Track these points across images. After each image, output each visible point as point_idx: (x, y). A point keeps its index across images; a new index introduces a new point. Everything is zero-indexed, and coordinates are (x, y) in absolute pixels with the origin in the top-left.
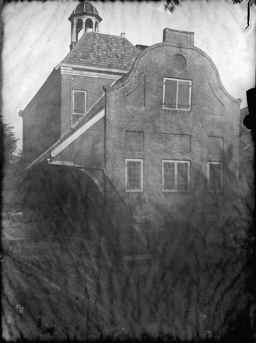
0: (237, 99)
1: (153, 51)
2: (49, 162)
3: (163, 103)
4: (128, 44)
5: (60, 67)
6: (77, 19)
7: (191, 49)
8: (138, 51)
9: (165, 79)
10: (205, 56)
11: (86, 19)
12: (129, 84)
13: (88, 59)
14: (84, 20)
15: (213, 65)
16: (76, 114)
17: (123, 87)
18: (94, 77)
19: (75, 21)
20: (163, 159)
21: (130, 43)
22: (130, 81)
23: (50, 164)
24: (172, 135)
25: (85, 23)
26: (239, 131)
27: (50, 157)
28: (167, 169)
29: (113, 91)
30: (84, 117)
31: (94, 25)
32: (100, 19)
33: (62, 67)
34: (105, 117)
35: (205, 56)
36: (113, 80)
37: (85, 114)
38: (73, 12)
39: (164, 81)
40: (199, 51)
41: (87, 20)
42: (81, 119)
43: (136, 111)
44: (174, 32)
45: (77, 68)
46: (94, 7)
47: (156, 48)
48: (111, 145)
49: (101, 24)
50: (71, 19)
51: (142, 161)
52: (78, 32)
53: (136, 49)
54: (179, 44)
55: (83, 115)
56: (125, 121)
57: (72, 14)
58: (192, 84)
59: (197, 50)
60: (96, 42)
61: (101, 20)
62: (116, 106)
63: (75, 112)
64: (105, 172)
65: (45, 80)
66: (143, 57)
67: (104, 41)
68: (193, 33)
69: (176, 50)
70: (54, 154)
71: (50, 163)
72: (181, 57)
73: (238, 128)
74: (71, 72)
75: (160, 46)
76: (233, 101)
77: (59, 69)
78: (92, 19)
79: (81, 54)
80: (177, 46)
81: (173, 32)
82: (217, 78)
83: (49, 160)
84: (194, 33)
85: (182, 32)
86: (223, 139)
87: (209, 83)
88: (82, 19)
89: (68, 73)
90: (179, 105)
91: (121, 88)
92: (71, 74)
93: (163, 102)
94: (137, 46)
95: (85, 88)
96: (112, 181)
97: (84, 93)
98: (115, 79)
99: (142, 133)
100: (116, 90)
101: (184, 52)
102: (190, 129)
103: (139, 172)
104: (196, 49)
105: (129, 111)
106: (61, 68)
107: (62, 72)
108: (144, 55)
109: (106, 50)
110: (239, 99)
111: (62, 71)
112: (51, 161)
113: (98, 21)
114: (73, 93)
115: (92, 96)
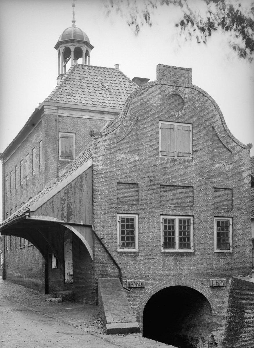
0: (247, 145)
1: (145, 91)
2: (27, 217)
5: (43, 107)
6: (64, 47)
7: (189, 88)
8: (135, 85)
9: (161, 122)
10: (205, 96)
12: (120, 130)
14: (72, 49)
15: (216, 107)
16: (62, 160)
17: (112, 133)
18: (84, 117)
19: (62, 50)
22: (120, 126)
23: (28, 219)
24: (172, 187)
26: (250, 181)
28: (167, 225)
29: (101, 137)
31: (84, 54)
32: (92, 47)
33: (46, 106)
35: (205, 96)
36: (107, 121)
39: (160, 125)
40: (199, 90)
43: (129, 160)
44: (169, 68)
45: (63, 107)
47: (149, 87)
49: (92, 53)
50: (57, 47)
51: (137, 216)
52: (66, 62)
54: (175, 83)
55: (72, 162)
59: (197, 89)
61: (93, 48)
62: (104, 154)
63: (62, 158)
66: (135, 98)
68: (191, 69)
69: (171, 90)
71: (29, 218)
73: (250, 178)
74: (56, 111)
75: (153, 84)
76: (241, 147)
77: (42, 109)
78: (81, 48)
80: (173, 85)
82: (222, 122)
83: (27, 214)
84: (191, 69)
85: (178, 68)
87: (213, 127)
88: (70, 47)
89: (52, 113)
90: (178, 153)
91: (110, 133)
93: (160, 150)
94: (135, 79)
95: (73, 130)
96: (102, 239)
97: (73, 135)
98: (108, 119)
100: (105, 136)
101: (182, 91)
102: (192, 180)
103: (228, 229)
104: (195, 88)
105: (120, 159)
106: (45, 107)
107: (46, 112)
108: (135, 96)
111: (45, 110)
112: (29, 216)
113: (89, 49)
115: (81, 139)
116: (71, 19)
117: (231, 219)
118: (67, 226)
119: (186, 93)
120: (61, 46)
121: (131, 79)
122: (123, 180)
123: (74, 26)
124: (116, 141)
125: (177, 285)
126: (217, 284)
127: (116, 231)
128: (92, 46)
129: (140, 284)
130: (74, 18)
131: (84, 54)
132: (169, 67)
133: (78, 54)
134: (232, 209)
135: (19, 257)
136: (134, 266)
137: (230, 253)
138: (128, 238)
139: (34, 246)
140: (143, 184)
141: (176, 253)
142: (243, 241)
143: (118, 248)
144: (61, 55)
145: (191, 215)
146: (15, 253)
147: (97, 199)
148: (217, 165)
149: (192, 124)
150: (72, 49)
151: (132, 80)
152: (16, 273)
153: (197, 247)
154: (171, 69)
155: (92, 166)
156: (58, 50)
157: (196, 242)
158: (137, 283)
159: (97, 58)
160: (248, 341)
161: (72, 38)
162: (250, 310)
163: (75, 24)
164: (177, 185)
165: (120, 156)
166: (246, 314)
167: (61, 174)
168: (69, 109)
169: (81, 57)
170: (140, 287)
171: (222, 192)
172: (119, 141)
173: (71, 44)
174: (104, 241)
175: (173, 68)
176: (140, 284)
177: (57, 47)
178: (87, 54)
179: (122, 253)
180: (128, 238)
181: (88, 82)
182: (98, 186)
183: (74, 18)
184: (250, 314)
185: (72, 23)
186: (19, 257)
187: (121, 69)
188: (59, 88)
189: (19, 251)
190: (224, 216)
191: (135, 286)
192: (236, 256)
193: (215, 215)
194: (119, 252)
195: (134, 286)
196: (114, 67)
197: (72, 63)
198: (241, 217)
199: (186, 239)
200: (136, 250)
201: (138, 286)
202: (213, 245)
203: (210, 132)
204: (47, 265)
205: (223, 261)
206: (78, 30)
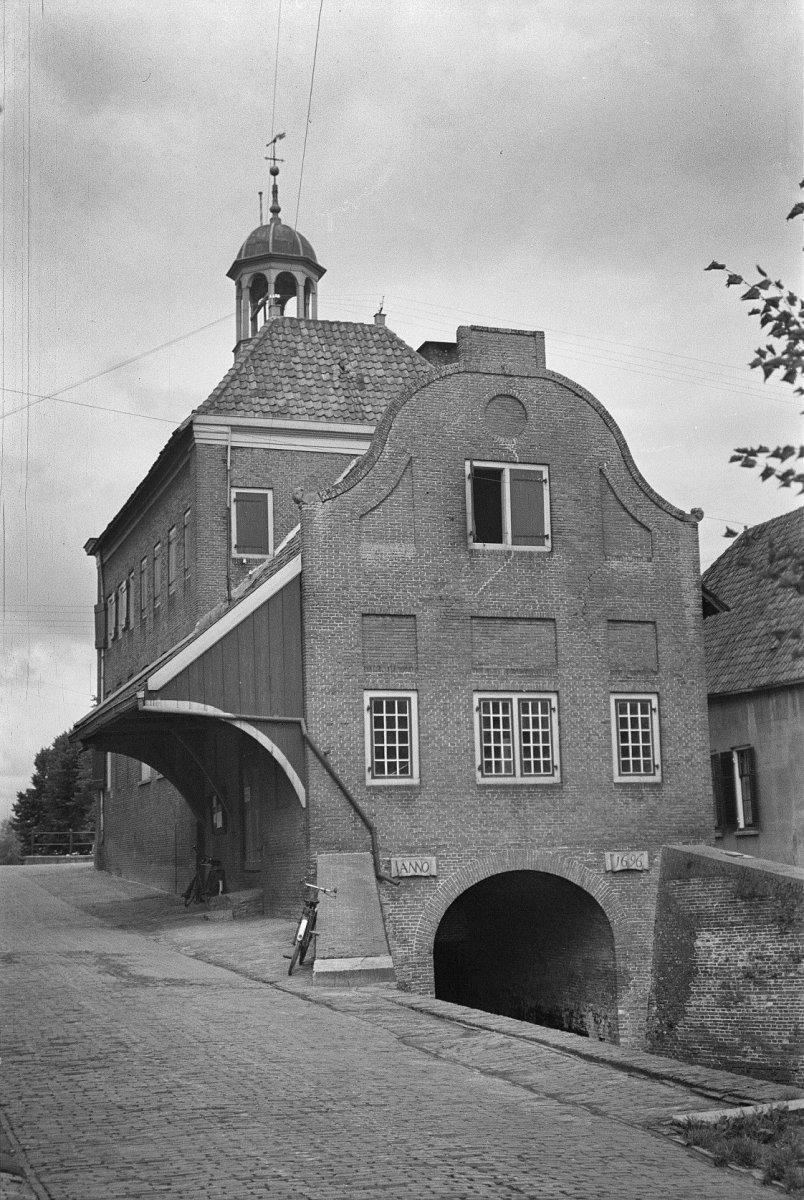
3: (469, 532)
4: (395, 344)
11: (278, 272)
13: (274, 399)
14: (272, 275)
19: (246, 280)
20: (478, 691)
21: (401, 343)
25: (276, 285)
27: (146, 690)
30: (265, 565)
31: (301, 290)
32: (321, 272)
34: (299, 580)
37: (269, 558)
38: (240, 255)
41: (279, 277)
42: (255, 571)
46: (300, 235)
48: (321, 655)
49: (321, 285)
50: (233, 273)
53: (420, 359)
56: (358, 588)
57: (235, 262)
58: (549, 476)
60: (300, 346)
63: (238, 552)
64: (304, 729)
65: (156, 459)
67: (322, 342)
70: (157, 681)
72: (509, 401)
73: (697, 592)
79: (254, 385)
81: (484, 334)
84: (543, 332)
86: (656, 628)
87: (601, 470)
88: (266, 273)
92: (224, 443)
94: (427, 347)
96: (325, 754)
99: (412, 619)
107: (201, 436)
109: (328, 369)
110: (693, 511)
113: (314, 276)
114: (234, 496)
118: (238, 725)
119: (527, 391)
120: (244, 270)
121: (415, 345)
122: (378, 606)
123: (276, 220)
124: (359, 511)
125: (519, 867)
126: (624, 863)
127: (362, 736)
129: (425, 868)
131: (301, 290)
132: (487, 330)
133: (287, 286)
134: (656, 673)
136: (408, 821)
137: (655, 785)
138: (391, 752)
139: (168, 781)
140: (428, 616)
141: (515, 786)
142: (686, 754)
143: (368, 776)
144: (246, 294)
145: (552, 689)
147: (312, 656)
148: (615, 564)
149: (548, 465)
151: (419, 351)
153: (568, 769)
154: (490, 335)
155: (301, 574)
157: (566, 757)
158: (417, 864)
159: (337, 301)
160: (706, 1013)
162: (708, 930)
163: (280, 215)
164: (514, 616)
165: (369, 551)
166: (698, 943)
167: (235, 593)
169: (294, 293)
170: (424, 874)
171: (626, 633)
172: (367, 513)
174: (332, 760)
175: (496, 331)
176: (425, 868)
177: (233, 273)
178: (309, 287)
179: (378, 790)
180: (391, 752)
181: (305, 361)
182: (315, 625)
184: (708, 941)
187: (390, 324)
188: (233, 379)
190: (637, 689)
191: (412, 873)
192: (668, 791)
193: (613, 688)
194: (369, 788)
195: (409, 874)
196: (372, 321)
197: (237, 336)
198: (679, 693)
199: (735, 760)
200: (415, 781)
201: (419, 873)
202: (611, 765)
203: (594, 484)
204: (202, 829)
205: (634, 809)
206: (290, 233)
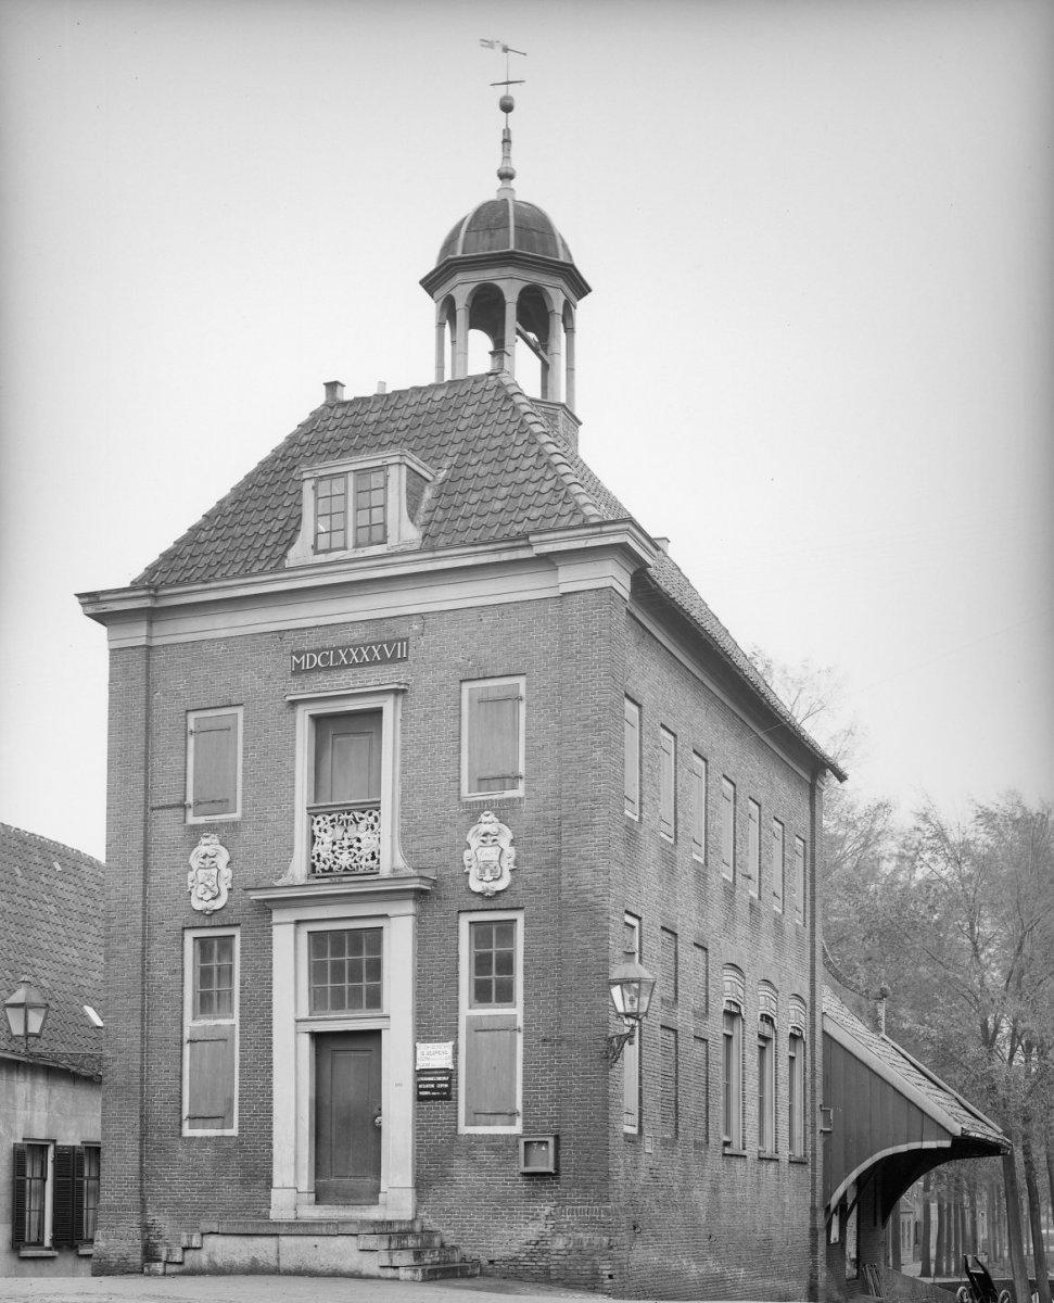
14: (511, 292)
32: (581, 289)
50: (431, 283)
88: (501, 284)
116: (497, 164)
117: (189, 936)
120: (459, 277)
128: (586, 285)
130: (507, 158)
135: (715, 1190)
146: (694, 1168)
150: (511, 292)
152: (700, 1260)
156: (441, 293)
161: (512, 247)
163: (514, 183)
168: (605, 529)
173: (509, 271)
177: (431, 283)
183: (507, 158)
185: (499, 183)
186: (715, 1190)
189: (715, 1162)
